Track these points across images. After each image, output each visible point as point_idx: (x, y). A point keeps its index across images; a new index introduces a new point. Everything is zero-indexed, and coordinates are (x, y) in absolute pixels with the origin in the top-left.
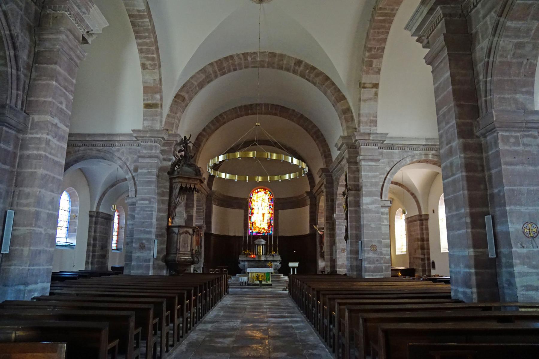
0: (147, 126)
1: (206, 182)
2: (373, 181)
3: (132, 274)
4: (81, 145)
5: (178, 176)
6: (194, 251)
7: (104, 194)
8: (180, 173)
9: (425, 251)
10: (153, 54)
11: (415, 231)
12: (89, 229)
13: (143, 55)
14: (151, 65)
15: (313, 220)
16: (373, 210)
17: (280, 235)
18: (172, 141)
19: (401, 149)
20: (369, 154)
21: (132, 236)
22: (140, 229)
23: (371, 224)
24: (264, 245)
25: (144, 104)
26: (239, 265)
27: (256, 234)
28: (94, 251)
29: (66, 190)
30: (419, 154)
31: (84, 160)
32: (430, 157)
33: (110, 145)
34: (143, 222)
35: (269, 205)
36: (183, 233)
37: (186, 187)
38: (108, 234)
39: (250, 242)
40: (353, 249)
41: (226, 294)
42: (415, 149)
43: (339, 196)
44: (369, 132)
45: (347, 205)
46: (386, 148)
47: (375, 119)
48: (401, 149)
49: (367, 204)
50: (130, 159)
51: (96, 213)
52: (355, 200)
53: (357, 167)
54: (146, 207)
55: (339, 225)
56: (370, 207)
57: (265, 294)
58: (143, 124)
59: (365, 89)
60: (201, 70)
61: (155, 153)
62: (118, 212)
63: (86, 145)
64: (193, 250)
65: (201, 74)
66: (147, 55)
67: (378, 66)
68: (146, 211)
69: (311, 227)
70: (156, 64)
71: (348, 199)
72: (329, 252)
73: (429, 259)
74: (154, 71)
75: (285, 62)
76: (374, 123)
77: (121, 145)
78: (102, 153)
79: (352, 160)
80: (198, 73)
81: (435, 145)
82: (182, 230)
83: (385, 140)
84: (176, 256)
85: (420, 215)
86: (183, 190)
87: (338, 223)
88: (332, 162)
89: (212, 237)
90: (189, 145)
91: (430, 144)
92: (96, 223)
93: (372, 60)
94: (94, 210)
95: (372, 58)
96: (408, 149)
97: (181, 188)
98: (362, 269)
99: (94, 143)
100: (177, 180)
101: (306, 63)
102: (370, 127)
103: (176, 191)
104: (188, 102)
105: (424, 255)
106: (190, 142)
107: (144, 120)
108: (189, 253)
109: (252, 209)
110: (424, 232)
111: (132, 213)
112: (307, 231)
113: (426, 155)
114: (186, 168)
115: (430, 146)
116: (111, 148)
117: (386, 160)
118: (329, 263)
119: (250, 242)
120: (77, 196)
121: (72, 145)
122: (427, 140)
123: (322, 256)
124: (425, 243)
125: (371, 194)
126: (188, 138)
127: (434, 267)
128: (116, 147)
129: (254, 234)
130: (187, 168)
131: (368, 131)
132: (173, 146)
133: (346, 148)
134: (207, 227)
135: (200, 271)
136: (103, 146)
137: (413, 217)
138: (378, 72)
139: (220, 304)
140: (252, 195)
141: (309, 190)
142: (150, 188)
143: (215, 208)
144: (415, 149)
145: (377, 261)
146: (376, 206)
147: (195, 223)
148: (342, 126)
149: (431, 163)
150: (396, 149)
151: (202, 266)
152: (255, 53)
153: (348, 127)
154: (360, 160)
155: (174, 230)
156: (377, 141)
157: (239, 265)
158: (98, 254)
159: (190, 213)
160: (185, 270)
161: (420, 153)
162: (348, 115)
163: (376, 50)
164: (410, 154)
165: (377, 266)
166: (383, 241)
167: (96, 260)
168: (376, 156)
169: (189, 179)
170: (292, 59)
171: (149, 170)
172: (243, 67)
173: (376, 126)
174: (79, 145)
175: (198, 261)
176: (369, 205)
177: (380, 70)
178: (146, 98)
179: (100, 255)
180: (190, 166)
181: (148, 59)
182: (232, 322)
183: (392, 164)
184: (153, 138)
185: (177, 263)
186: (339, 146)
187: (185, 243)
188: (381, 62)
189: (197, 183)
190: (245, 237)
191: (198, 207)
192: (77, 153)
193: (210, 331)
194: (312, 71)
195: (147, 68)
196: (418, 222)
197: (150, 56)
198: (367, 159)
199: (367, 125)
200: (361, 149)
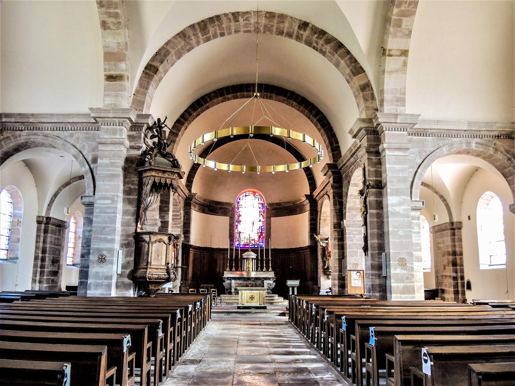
0: (109, 104)
1: (185, 177)
2: (401, 175)
3: (88, 295)
4: (23, 128)
5: (150, 168)
6: (170, 265)
7: (56, 195)
8: (152, 164)
9: (458, 268)
10: (116, 8)
11: (443, 243)
12: (37, 239)
13: (103, 10)
14: (114, 24)
15: (314, 229)
16: (401, 212)
17: (272, 248)
18: (141, 123)
19: (436, 135)
20: (395, 141)
21: (89, 246)
22: (99, 236)
23: (398, 231)
24: (255, 259)
25: (105, 75)
26: (224, 283)
27: (244, 246)
28: (42, 267)
29: (6, 188)
30: (458, 143)
31: (27, 148)
32: (473, 146)
33: (61, 129)
34: (104, 228)
35: (260, 212)
36: (155, 242)
37: (160, 183)
38: (60, 246)
39: (237, 256)
40: (374, 263)
41: (210, 320)
42: (453, 136)
43: (350, 198)
44: (396, 113)
45: (366, 207)
46: (416, 135)
47: (402, 96)
48: (436, 135)
49: (393, 205)
50: (87, 146)
51: (45, 219)
52: (376, 201)
53: (378, 158)
54: (107, 207)
55: (350, 234)
56: (397, 209)
57: (258, 319)
58: (104, 101)
59: (390, 58)
60: (178, 34)
61: (119, 138)
62: (75, 218)
63: (29, 129)
64: (168, 263)
65: (179, 39)
66: (109, 10)
67: (409, 27)
68: (108, 213)
69: (312, 238)
70: (120, 22)
71: (368, 200)
72: (338, 268)
73: (462, 278)
74: (117, 31)
75: (287, 25)
76: (401, 101)
77: (76, 128)
78: (50, 139)
79: (372, 149)
80: (174, 37)
81: (480, 131)
82: (154, 238)
83: (415, 124)
84: (146, 272)
85: (452, 223)
86: (157, 187)
87: (349, 232)
88: (341, 156)
89: (191, 249)
90: (163, 129)
91: (474, 129)
92: (46, 232)
93: (401, 18)
94: (44, 214)
95: (401, 16)
96: (445, 136)
97: (154, 183)
98: (386, 290)
99: (40, 126)
100: (148, 174)
101: (313, 26)
102: (396, 107)
103: (147, 188)
104: (163, 75)
105: (456, 272)
106: (166, 126)
107: (105, 96)
108: (163, 267)
109: (239, 216)
110: (457, 243)
111: (89, 216)
112: (305, 241)
113: (468, 143)
114: (160, 159)
115: (473, 132)
116: (62, 132)
117: (416, 150)
118: (337, 282)
119: (237, 256)
120: (21, 197)
121: (12, 128)
122: (470, 124)
123: (326, 272)
124: (458, 257)
125: (398, 193)
126: (162, 121)
127: (469, 287)
128: (68, 131)
129: (241, 246)
130: (162, 159)
131: (394, 112)
132: (144, 130)
133: (365, 134)
134: (185, 237)
135: (177, 291)
136: (52, 129)
137: (441, 225)
138: (409, 34)
139: (203, 334)
140: (240, 199)
141: (309, 194)
142: (112, 183)
143: (196, 215)
144: (453, 136)
145: (407, 278)
146: (404, 207)
147: (171, 230)
148: (358, 106)
149: (473, 155)
150: (429, 136)
151: (179, 285)
152: (247, 13)
153: (367, 108)
154: (384, 150)
155: (145, 238)
156: (406, 125)
157: (224, 283)
158: (49, 270)
159: (165, 219)
160: (157, 290)
161: (460, 141)
162: (367, 92)
163: (407, 5)
164: (447, 141)
165: (407, 285)
166: (414, 253)
167: (45, 278)
168: (405, 143)
169: (164, 172)
170: (296, 20)
171: (112, 161)
172: (233, 31)
173: (404, 106)
174: (20, 129)
175: (176, 277)
176: (395, 206)
177: (410, 32)
178: (107, 67)
179: (50, 272)
180: (164, 156)
181: (110, 15)
182: (223, 361)
183: (424, 155)
184: (117, 120)
185: (148, 280)
186: (355, 133)
187: (158, 256)
188: (413, 22)
189: (174, 177)
190: (232, 250)
191: (175, 213)
192: (19, 139)
193: (193, 376)
194: (321, 36)
195: (109, 28)
196: (449, 232)
197: (112, 11)
198: (393, 147)
199: (392, 105)
200: (384, 135)
